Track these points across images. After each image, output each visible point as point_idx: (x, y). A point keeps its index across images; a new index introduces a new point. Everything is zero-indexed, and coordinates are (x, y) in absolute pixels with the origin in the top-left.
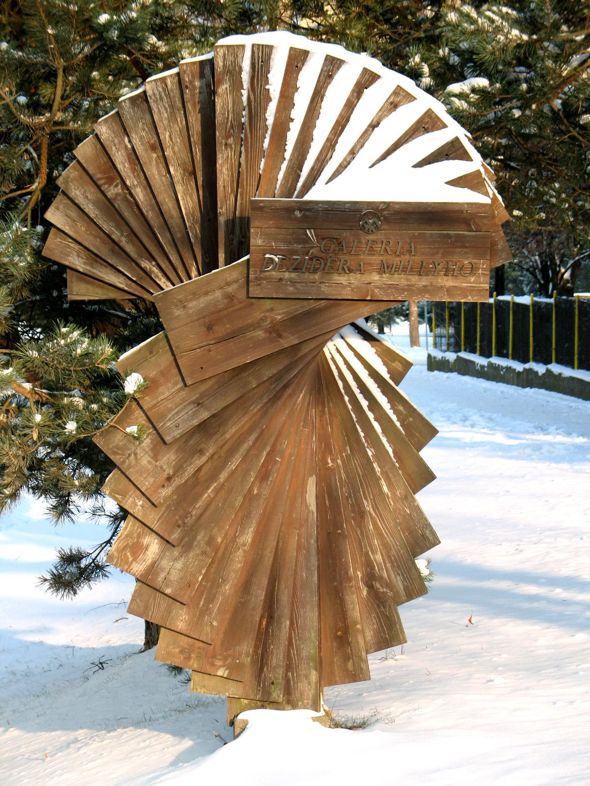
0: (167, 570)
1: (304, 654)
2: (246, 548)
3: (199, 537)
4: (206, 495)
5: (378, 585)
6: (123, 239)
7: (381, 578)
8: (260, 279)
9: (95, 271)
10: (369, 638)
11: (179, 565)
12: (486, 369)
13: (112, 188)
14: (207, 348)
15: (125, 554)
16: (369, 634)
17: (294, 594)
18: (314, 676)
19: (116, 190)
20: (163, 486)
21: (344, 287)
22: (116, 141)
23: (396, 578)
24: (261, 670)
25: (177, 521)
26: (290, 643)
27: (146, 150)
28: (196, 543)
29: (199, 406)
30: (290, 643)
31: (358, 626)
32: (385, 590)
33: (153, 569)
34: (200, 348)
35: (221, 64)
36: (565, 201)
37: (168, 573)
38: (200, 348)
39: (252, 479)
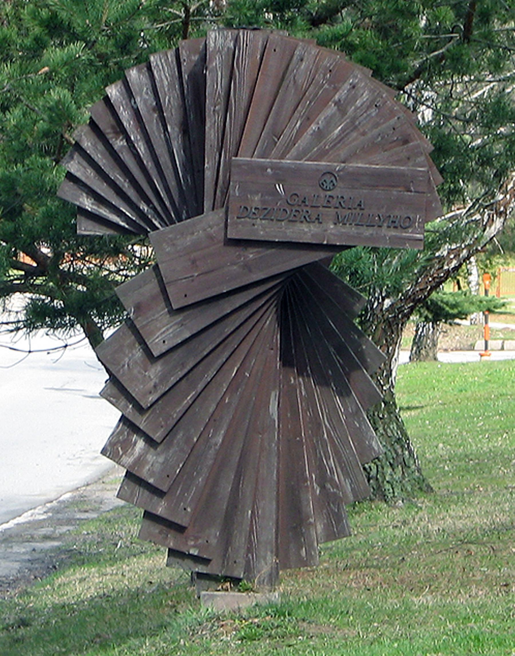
0: (151, 463)
1: (263, 538)
2: (217, 447)
3: (178, 437)
4: (186, 402)
5: (329, 486)
6: (126, 185)
7: (332, 480)
8: (237, 224)
9: (101, 211)
10: (319, 532)
11: (161, 459)
12: (49, 261)
13: (118, 141)
14: (191, 279)
15: (117, 449)
16: (320, 527)
17: (256, 489)
18: (271, 559)
19: (121, 143)
20: (150, 393)
21: (305, 233)
22: (124, 102)
23: (345, 480)
24: (226, 550)
25: (161, 422)
26: (251, 531)
27: (148, 112)
28: (175, 441)
29: (183, 327)
30: (251, 531)
31: (312, 520)
32: (335, 490)
33: (140, 461)
34: (185, 278)
35: (212, 45)
36: (140, 262)
37: (152, 465)
38: (185, 278)
39: (225, 390)
